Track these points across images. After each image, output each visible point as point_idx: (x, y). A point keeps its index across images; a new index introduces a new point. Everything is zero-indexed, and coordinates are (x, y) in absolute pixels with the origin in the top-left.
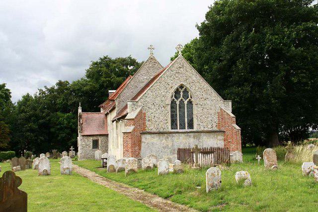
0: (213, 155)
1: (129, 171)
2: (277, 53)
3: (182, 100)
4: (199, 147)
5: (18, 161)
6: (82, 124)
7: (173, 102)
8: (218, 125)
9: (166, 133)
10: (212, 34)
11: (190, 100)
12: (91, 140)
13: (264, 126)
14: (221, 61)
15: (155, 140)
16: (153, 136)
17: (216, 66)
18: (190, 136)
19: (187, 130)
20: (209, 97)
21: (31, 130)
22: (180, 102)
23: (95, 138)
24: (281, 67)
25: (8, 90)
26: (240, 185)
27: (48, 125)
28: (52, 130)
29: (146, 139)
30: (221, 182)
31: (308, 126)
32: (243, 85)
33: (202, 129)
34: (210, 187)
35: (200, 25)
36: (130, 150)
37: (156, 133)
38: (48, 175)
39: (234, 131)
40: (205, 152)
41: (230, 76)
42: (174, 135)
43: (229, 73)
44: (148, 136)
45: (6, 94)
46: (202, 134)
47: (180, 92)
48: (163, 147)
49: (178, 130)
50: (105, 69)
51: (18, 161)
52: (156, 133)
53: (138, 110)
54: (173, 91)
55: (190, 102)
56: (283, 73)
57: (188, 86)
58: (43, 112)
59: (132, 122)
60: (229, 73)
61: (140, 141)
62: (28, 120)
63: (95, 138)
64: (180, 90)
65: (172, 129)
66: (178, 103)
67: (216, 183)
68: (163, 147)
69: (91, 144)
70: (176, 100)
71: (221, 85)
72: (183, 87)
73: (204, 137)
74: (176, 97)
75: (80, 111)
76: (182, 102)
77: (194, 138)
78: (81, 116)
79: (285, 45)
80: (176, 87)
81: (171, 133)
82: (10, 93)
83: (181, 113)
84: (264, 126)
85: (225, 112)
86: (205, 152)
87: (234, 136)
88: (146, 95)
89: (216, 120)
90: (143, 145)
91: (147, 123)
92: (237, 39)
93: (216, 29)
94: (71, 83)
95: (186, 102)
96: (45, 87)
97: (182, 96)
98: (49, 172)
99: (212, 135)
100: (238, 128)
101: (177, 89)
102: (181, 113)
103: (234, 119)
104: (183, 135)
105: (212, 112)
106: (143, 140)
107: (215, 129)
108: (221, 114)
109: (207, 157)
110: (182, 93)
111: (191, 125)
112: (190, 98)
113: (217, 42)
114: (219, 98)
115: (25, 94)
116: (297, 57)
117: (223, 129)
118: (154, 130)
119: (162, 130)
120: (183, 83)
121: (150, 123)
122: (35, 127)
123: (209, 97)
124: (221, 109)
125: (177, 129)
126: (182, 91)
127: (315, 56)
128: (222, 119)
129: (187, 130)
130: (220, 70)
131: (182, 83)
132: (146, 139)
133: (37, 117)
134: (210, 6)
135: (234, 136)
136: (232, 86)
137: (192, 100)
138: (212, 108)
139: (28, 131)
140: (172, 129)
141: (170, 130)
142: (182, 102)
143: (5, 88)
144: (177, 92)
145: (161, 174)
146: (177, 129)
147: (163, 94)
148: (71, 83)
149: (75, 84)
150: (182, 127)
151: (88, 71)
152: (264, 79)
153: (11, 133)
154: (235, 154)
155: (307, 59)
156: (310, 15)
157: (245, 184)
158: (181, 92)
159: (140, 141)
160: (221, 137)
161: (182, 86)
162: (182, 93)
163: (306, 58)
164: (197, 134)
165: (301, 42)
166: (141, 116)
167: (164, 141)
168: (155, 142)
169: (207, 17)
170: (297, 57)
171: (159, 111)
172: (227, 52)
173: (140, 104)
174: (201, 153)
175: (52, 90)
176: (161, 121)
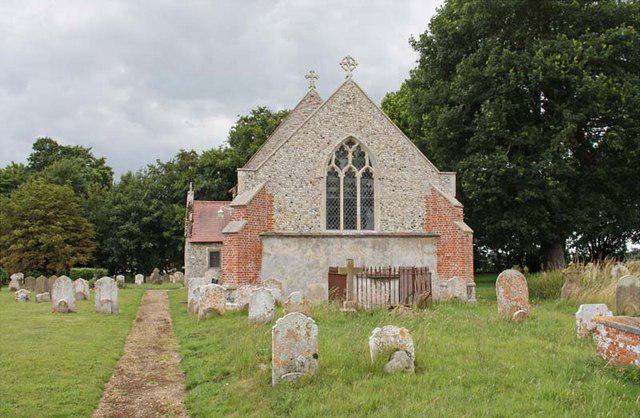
0: (397, 282)
1: (205, 312)
2: (559, 89)
3: (350, 169)
4: (357, 264)
5: (46, 284)
6: (193, 221)
7: (332, 173)
8: (427, 223)
9: (315, 237)
10: (439, 56)
11: (367, 169)
12: (207, 253)
13: (521, 225)
14: (452, 104)
15: (291, 249)
16: (286, 240)
17: (444, 113)
18: (365, 245)
19: (342, 231)
20: (407, 163)
21: (130, 235)
22: (363, 174)
23: (214, 248)
24: (567, 114)
25: (108, 169)
26: (377, 369)
27: (128, 227)
28: (166, 234)
29: (272, 247)
30: (316, 356)
31: (624, 237)
32: (493, 150)
33: (392, 230)
34: (282, 371)
35: (418, 39)
36: (235, 269)
37: (293, 236)
38: (69, 311)
39: (458, 236)
40: (380, 277)
41: (471, 133)
42: (332, 240)
43: (467, 128)
44: (277, 242)
45: (104, 175)
46: (392, 240)
47: (346, 153)
48: (308, 266)
49: (342, 231)
50: (259, 129)
51: (46, 284)
52: (293, 236)
53: (257, 189)
54: (331, 150)
55: (368, 175)
56: (571, 127)
57: (364, 141)
58: (150, 204)
59: (242, 212)
60: (467, 128)
61: (260, 251)
62: (125, 216)
63: (214, 248)
64: (347, 148)
65: (329, 228)
66: (342, 175)
67: (300, 358)
68: (308, 266)
69: (207, 259)
70: (337, 169)
71: (445, 151)
72: (353, 144)
73: (396, 247)
74: (337, 163)
75: (190, 197)
76: (350, 175)
77: (374, 247)
78: (190, 208)
79: (575, 71)
80: (339, 141)
81: (324, 236)
82: (112, 174)
83: (349, 202)
84: (521, 225)
85: (440, 195)
86: (380, 277)
87: (458, 246)
88: (275, 158)
89: (423, 213)
90: (265, 259)
91: (276, 215)
92: (481, 64)
93: (445, 49)
94: (200, 153)
95: (359, 174)
96: (159, 163)
97: (350, 162)
98: (71, 306)
99: (411, 242)
100: (466, 228)
101: (342, 147)
102: (349, 202)
103: (460, 211)
104: (350, 241)
105: (414, 195)
106: (266, 249)
107: (420, 230)
108: (433, 200)
109: (383, 287)
110: (350, 156)
111: (367, 222)
112: (367, 165)
113: (447, 70)
114: (430, 167)
115: (125, 173)
116: (599, 95)
117: (435, 231)
118: (290, 231)
119: (306, 231)
120: (353, 135)
121: (281, 215)
122: (136, 229)
123: (407, 163)
124: (433, 190)
125: (338, 228)
126: (350, 150)
127: (634, 94)
128: (435, 210)
129: (359, 231)
130: (451, 122)
131: (351, 134)
132: (272, 247)
133: (141, 213)
134: (439, 8)
135: (458, 246)
136: (473, 152)
137: (372, 169)
138: (416, 189)
139: (124, 236)
140: (329, 228)
141: (324, 230)
142: (350, 175)
143: (105, 165)
144: (341, 153)
145: (255, 321)
146: (338, 228)
147: (311, 156)
148: (200, 153)
149: (206, 155)
150: (350, 224)
151: (232, 133)
152: (534, 138)
153: (97, 238)
154: (453, 285)
155: (620, 101)
156: (624, 16)
157: (394, 364)
158: (350, 152)
159: (259, 252)
160: (430, 247)
161: (350, 142)
162: (350, 156)
163: (616, 98)
164: (380, 240)
165: (607, 66)
166: (263, 200)
167: (310, 252)
168: (291, 254)
169: (431, 25)
170: (599, 95)
171: (301, 190)
172: (465, 86)
173: (261, 175)
174: (370, 277)
175: (168, 167)
176: (306, 213)
